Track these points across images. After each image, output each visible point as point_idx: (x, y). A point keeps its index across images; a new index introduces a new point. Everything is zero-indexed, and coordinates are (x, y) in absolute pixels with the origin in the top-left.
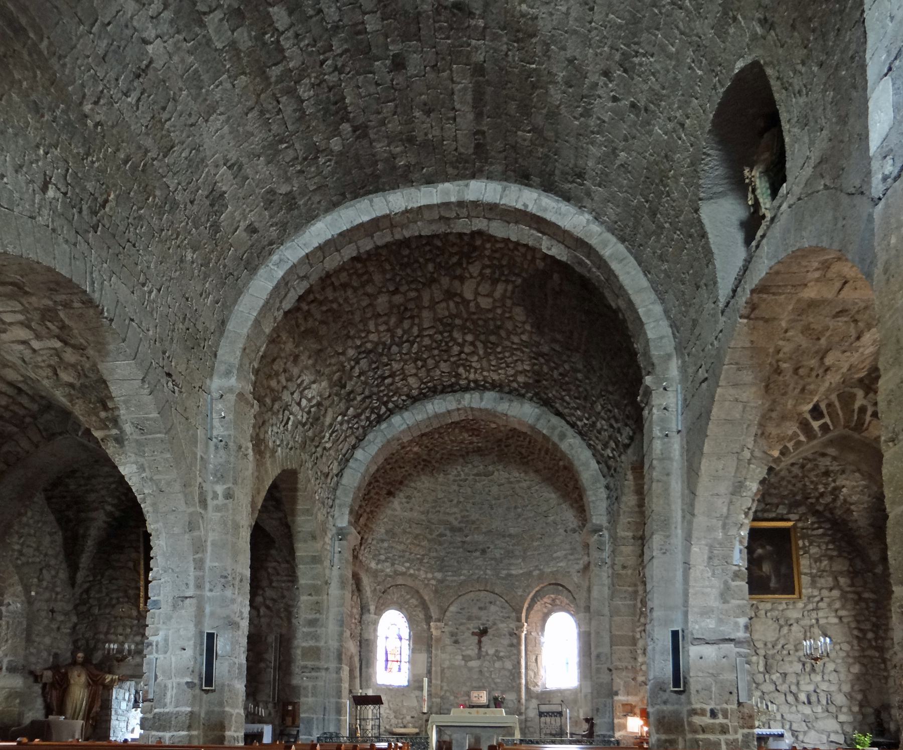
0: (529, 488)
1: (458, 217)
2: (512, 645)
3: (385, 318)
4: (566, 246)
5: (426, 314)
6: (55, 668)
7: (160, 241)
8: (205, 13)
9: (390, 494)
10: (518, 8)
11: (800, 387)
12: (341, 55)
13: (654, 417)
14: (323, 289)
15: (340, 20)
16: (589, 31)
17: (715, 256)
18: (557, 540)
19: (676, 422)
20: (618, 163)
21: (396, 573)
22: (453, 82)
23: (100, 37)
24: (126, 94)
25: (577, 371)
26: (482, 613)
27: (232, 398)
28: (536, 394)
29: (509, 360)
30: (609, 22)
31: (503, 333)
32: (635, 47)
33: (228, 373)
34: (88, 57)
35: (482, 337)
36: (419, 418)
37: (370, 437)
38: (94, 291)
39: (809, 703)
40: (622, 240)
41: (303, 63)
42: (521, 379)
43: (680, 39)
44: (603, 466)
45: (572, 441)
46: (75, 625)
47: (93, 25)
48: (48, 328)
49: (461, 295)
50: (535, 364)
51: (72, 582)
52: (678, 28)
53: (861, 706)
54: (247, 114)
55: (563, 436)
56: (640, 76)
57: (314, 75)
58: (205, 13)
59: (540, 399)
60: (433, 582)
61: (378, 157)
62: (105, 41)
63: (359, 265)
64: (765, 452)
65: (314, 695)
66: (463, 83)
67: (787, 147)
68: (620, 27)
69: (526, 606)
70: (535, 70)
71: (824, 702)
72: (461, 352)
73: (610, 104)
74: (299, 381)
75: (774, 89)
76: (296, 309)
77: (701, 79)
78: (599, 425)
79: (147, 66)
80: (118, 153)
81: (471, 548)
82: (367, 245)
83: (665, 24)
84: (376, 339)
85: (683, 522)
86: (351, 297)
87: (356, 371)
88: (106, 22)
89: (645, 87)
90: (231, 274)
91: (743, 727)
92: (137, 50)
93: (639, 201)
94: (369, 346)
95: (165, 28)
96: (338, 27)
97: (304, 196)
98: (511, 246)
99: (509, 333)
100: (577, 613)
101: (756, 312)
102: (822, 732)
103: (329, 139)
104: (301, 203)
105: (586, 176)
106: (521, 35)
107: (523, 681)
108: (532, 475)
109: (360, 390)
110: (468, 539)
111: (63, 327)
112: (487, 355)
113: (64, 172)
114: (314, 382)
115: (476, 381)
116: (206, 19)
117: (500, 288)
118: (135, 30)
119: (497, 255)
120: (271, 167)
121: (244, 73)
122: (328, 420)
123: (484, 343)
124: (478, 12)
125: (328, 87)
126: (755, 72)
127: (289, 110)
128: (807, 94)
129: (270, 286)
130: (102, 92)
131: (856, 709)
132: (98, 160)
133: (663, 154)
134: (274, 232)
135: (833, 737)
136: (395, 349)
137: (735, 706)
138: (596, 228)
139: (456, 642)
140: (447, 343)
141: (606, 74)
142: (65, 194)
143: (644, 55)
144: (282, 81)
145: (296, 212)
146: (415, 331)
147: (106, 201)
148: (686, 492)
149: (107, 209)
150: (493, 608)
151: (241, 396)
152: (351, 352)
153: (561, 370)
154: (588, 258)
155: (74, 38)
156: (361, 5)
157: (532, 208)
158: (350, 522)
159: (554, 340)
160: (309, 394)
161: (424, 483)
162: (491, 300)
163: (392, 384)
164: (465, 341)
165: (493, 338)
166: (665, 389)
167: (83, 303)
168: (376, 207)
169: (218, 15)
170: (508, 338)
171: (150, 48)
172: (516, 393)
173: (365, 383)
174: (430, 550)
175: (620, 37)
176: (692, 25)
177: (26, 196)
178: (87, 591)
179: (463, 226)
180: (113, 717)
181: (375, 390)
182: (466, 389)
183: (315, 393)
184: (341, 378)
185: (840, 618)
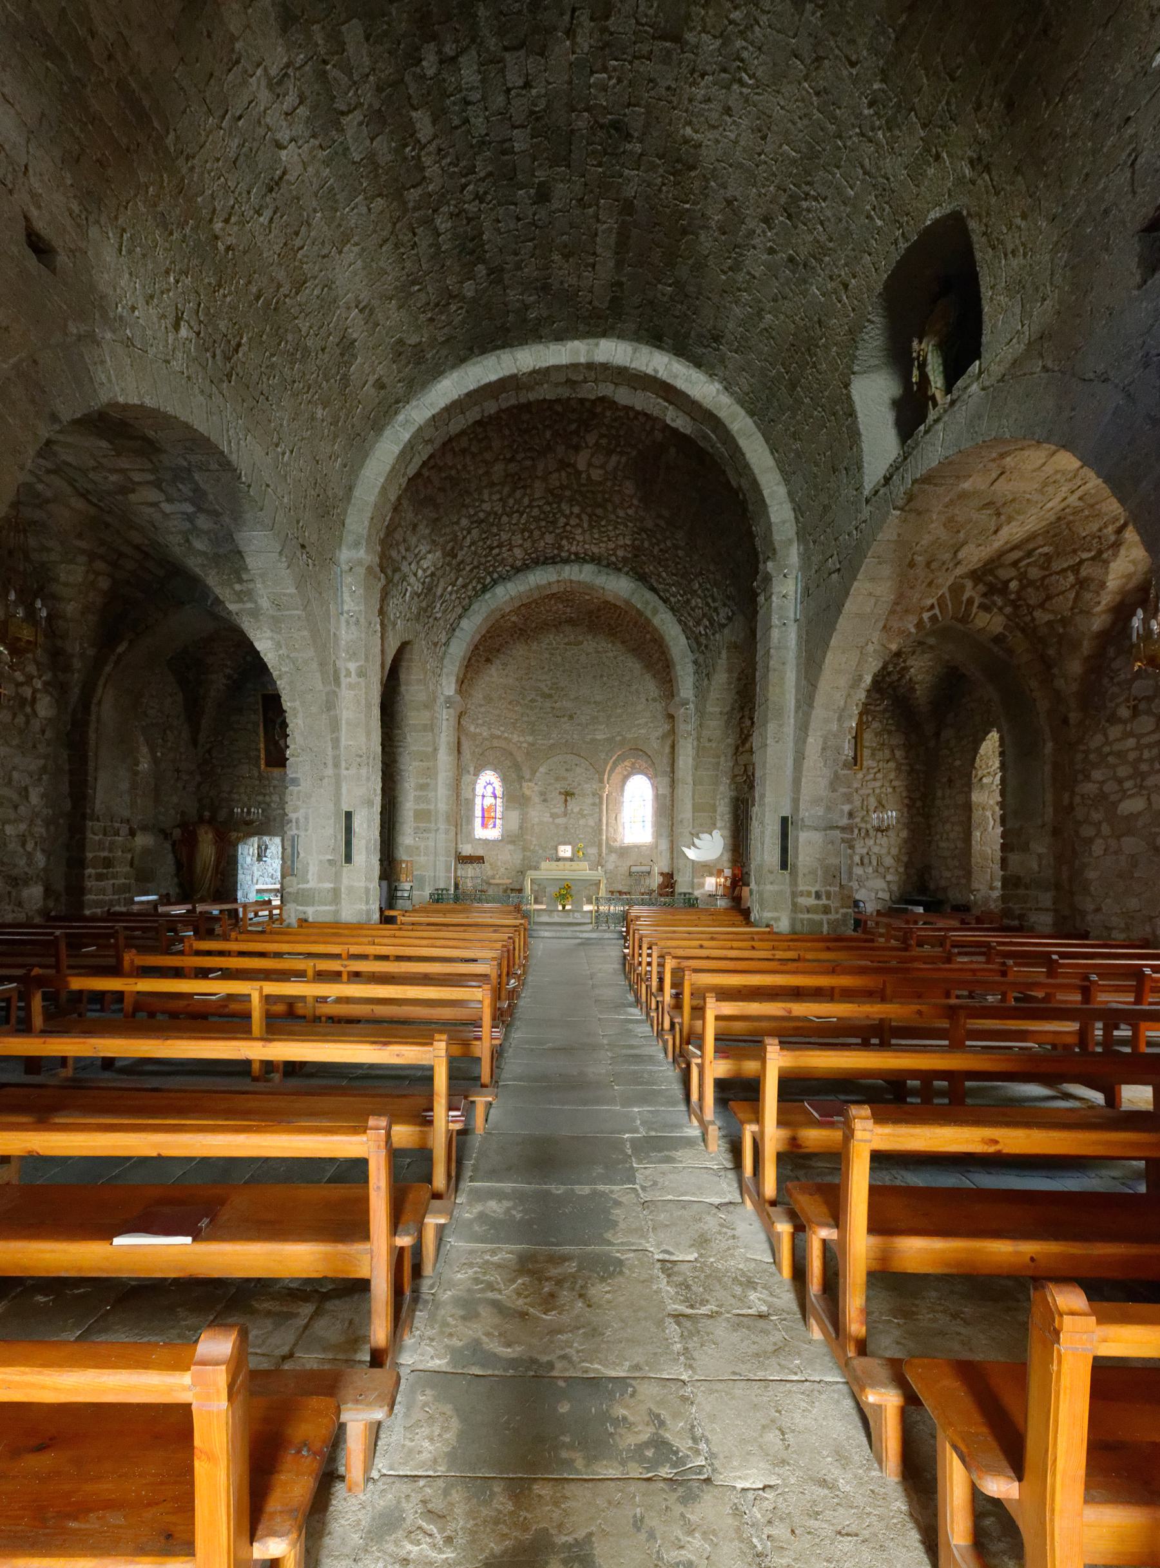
0: (615, 658)
1: (585, 381)
2: (594, 804)
3: (498, 488)
4: (692, 418)
5: (538, 484)
6: (183, 825)
7: (293, 395)
8: (343, 113)
9: (488, 660)
10: (681, 132)
11: (929, 580)
12: (483, 180)
13: (774, 605)
14: (444, 454)
15: (487, 135)
16: (757, 166)
17: (863, 438)
18: (639, 708)
20: (762, 326)
21: (493, 737)
22: (598, 221)
23: (230, 133)
25: (676, 547)
27: (361, 571)
28: (631, 569)
29: (612, 534)
30: (782, 155)
31: (610, 507)
32: (807, 188)
33: (357, 544)
34: (218, 160)
35: (589, 510)
36: (522, 588)
37: (475, 607)
38: (231, 453)
39: (862, 864)
40: (751, 413)
41: (443, 187)
42: (620, 553)
43: (863, 181)
44: (692, 641)
45: (664, 616)
46: (200, 784)
47: (223, 117)
48: (180, 490)
49: (574, 466)
50: (636, 539)
51: (195, 743)
52: (862, 167)
53: (906, 867)
54: (381, 246)
55: (655, 611)
56: (805, 225)
57: (453, 202)
58: (343, 113)
59: (636, 573)
60: (525, 745)
61: (509, 308)
62: (236, 140)
64: (883, 645)
65: (425, 854)
66: (609, 223)
67: (985, 318)
68: (794, 162)
70: (688, 210)
71: (874, 863)
72: (567, 524)
73: (765, 257)
74: (416, 551)
75: (976, 246)
76: (418, 474)
77: (879, 230)
78: (693, 603)
79: (281, 178)
80: (250, 287)
82: (491, 407)
83: (848, 159)
84: (488, 509)
85: (796, 712)
86: (469, 463)
88: (237, 114)
89: (810, 238)
90: (359, 435)
91: (842, 907)
92: (269, 155)
93: (779, 372)
94: (482, 515)
95: (299, 129)
96: (483, 143)
97: (433, 348)
98: (631, 415)
99: (615, 508)
100: (656, 776)
101: (912, 504)
102: (871, 890)
103: (462, 282)
104: (429, 356)
105: (723, 341)
106: (679, 166)
108: (619, 645)
109: (469, 560)
110: (558, 705)
111: (197, 490)
112: (591, 527)
113: (195, 307)
114: (429, 552)
115: (576, 554)
116: (345, 120)
117: (614, 458)
118: (269, 129)
119: (616, 424)
120: (403, 312)
121: (380, 195)
122: (439, 591)
124: (636, 134)
125: (467, 218)
126: (955, 224)
127: (424, 245)
128: (1025, 255)
129: (396, 449)
130: (233, 207)
131: (901, 870)
132: (230, 293)
133: (816, 319)
134: (400, 388)
135: (880, 895)
136: (505, 519)
137: (837, 889)
138: (725, 399)
139: (545, 800)
140: (554, 514)
141: (767, 220)
142: (198, 334)
143: (815, 199)
144: (419, 209)
145: (423, 367)
146: (526, 501)
147: (239, 345)
148: (803, 682)
149: (240, 354)
151: (369, 569)
152: (464, 522)
153: (662, 546)
154: (714, 432)
155: (203, 133)
156: (511, 117)
157: (662, 374)
159: (659, 516)
160: (425, 564)
161: (520, 650)
162: (601, 472)
163: (498, 555)
164: (572, 513)
165: (599, 511)
166: (785, 576)
167: (220, 465)
168: (504, 365)
169: (357, 116)
170: (614, 512)
171: (284, 153)
173: (475, 553)
174: (522, 715)
175: (790, 175)
176: (881, 163)
177: (159, 335)
178: (209, 751)
179: (590, 391)
180: (240, 871)
181: (483, 560)
182: (566, 561)
183: (429, 564)
184: (453, 548)
185: (894, 788)
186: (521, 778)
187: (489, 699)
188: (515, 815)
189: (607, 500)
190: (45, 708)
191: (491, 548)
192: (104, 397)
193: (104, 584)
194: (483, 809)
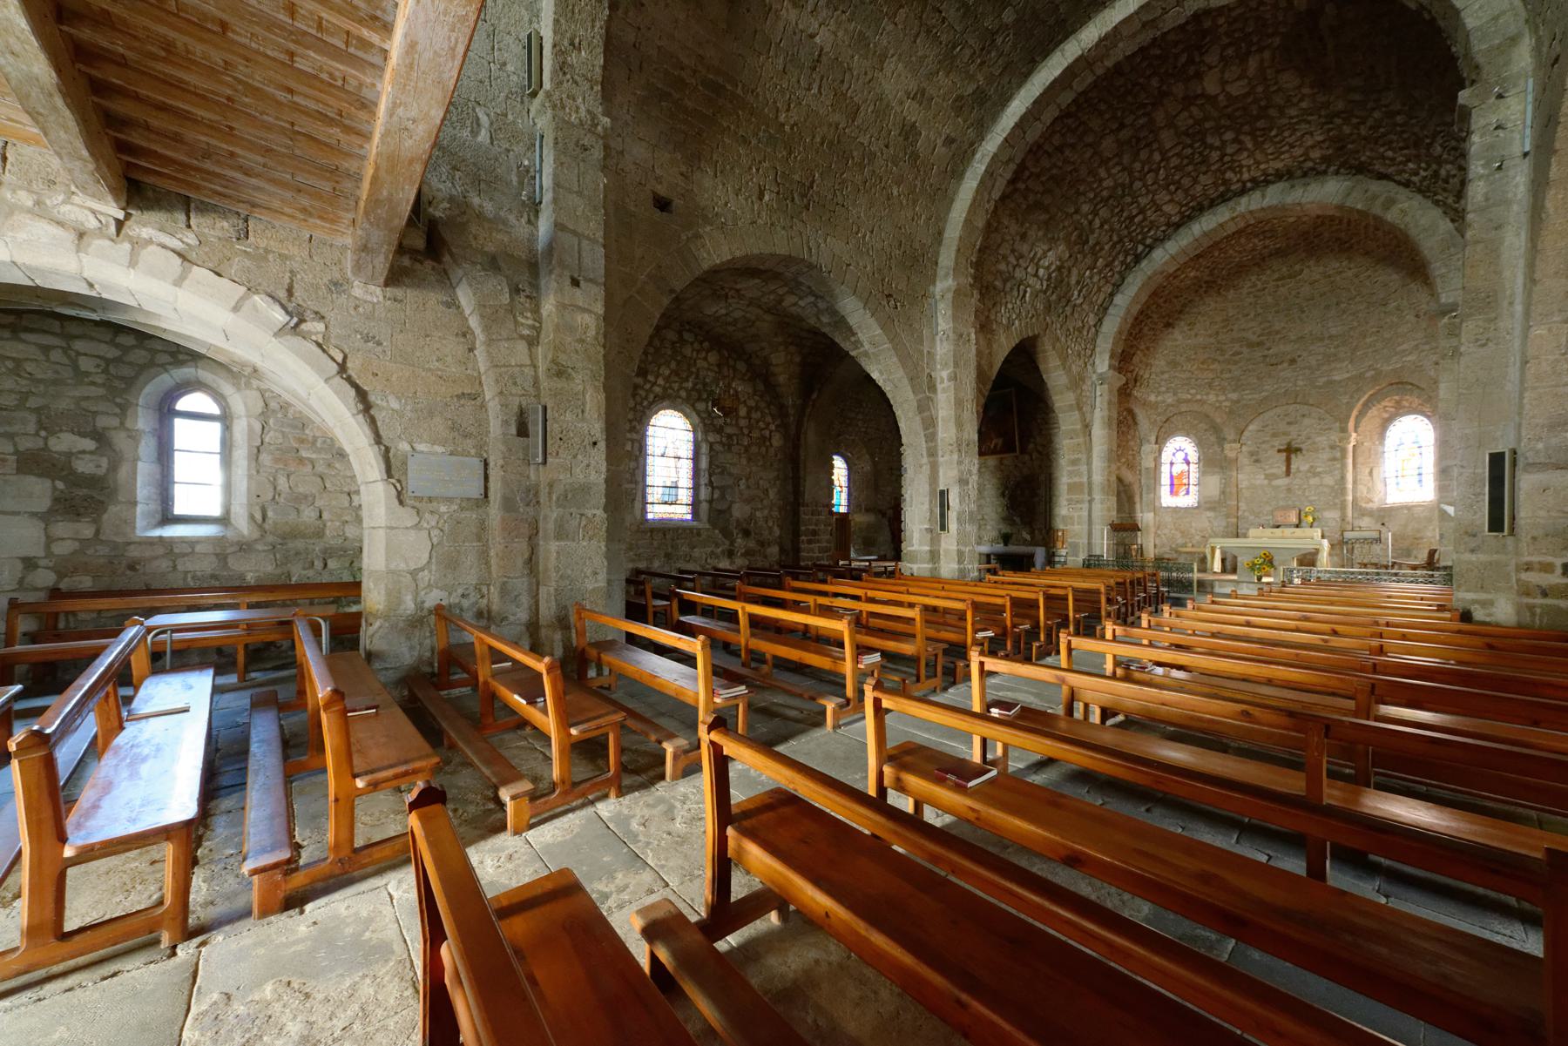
9: (1168, 325)
19: (1521, 139)
21: (1180, 402)
24: (809, 89)
26: (1291, 428)
29: (1290, 140)
31: (1273, 112)
36: (1184, 243)
37: (1129, 279)
42: (1316, 154)
50: (1330, 130)
63: (1070, 121)
69: (1355, 413)
78: (1443, 172)
81: (1274, 361)
82: (1066, 98)
87: (1097, 222)
107: (1350, 498)
112: (1258, 145)
115: (1253, 180)
117: (1253, 63)
121: (901, 6)
122: (1073, 280)
123: (1252, 134)
129: (975, 184)
134: (971, 133)
139: (1257, 461)
145: (988, 104)
146: (1157, 157)
150: (1306, 421)
152: (1085, 208)
153: (1370, 122)
158: (1110, 366)
162: (1244, 82)
172: (1316, 173)
182: (1243, 192)
184: (1080, 236)
186: (1221, 441)
187: (1174, 364)
188: (1214, 482)
189: (1267, 107)
190: (777, 441)
191: (1131, 218)
192: (706, 266)
193: (797, 359)
194: (1172, 477)
